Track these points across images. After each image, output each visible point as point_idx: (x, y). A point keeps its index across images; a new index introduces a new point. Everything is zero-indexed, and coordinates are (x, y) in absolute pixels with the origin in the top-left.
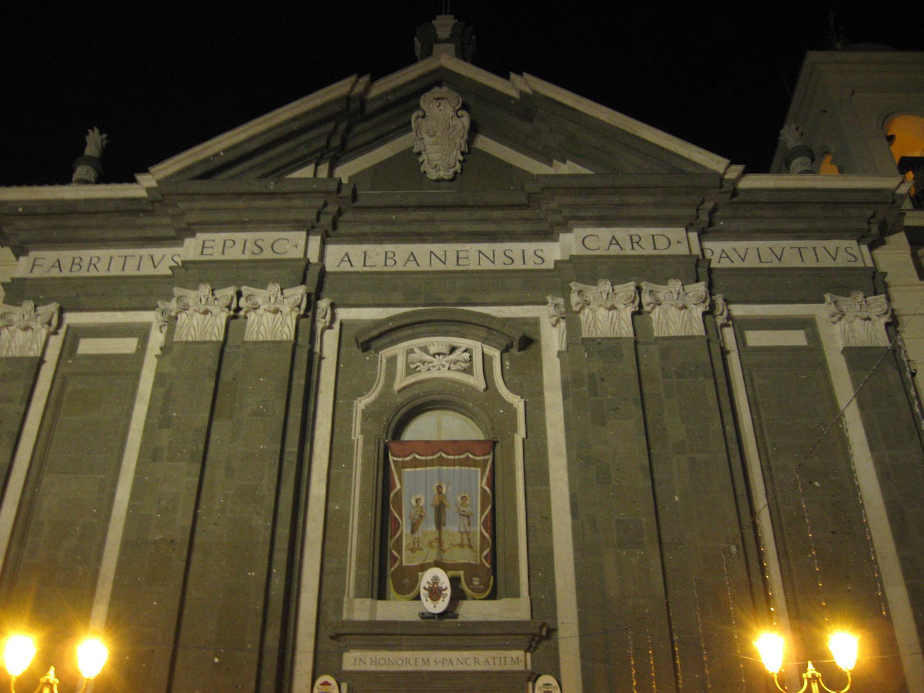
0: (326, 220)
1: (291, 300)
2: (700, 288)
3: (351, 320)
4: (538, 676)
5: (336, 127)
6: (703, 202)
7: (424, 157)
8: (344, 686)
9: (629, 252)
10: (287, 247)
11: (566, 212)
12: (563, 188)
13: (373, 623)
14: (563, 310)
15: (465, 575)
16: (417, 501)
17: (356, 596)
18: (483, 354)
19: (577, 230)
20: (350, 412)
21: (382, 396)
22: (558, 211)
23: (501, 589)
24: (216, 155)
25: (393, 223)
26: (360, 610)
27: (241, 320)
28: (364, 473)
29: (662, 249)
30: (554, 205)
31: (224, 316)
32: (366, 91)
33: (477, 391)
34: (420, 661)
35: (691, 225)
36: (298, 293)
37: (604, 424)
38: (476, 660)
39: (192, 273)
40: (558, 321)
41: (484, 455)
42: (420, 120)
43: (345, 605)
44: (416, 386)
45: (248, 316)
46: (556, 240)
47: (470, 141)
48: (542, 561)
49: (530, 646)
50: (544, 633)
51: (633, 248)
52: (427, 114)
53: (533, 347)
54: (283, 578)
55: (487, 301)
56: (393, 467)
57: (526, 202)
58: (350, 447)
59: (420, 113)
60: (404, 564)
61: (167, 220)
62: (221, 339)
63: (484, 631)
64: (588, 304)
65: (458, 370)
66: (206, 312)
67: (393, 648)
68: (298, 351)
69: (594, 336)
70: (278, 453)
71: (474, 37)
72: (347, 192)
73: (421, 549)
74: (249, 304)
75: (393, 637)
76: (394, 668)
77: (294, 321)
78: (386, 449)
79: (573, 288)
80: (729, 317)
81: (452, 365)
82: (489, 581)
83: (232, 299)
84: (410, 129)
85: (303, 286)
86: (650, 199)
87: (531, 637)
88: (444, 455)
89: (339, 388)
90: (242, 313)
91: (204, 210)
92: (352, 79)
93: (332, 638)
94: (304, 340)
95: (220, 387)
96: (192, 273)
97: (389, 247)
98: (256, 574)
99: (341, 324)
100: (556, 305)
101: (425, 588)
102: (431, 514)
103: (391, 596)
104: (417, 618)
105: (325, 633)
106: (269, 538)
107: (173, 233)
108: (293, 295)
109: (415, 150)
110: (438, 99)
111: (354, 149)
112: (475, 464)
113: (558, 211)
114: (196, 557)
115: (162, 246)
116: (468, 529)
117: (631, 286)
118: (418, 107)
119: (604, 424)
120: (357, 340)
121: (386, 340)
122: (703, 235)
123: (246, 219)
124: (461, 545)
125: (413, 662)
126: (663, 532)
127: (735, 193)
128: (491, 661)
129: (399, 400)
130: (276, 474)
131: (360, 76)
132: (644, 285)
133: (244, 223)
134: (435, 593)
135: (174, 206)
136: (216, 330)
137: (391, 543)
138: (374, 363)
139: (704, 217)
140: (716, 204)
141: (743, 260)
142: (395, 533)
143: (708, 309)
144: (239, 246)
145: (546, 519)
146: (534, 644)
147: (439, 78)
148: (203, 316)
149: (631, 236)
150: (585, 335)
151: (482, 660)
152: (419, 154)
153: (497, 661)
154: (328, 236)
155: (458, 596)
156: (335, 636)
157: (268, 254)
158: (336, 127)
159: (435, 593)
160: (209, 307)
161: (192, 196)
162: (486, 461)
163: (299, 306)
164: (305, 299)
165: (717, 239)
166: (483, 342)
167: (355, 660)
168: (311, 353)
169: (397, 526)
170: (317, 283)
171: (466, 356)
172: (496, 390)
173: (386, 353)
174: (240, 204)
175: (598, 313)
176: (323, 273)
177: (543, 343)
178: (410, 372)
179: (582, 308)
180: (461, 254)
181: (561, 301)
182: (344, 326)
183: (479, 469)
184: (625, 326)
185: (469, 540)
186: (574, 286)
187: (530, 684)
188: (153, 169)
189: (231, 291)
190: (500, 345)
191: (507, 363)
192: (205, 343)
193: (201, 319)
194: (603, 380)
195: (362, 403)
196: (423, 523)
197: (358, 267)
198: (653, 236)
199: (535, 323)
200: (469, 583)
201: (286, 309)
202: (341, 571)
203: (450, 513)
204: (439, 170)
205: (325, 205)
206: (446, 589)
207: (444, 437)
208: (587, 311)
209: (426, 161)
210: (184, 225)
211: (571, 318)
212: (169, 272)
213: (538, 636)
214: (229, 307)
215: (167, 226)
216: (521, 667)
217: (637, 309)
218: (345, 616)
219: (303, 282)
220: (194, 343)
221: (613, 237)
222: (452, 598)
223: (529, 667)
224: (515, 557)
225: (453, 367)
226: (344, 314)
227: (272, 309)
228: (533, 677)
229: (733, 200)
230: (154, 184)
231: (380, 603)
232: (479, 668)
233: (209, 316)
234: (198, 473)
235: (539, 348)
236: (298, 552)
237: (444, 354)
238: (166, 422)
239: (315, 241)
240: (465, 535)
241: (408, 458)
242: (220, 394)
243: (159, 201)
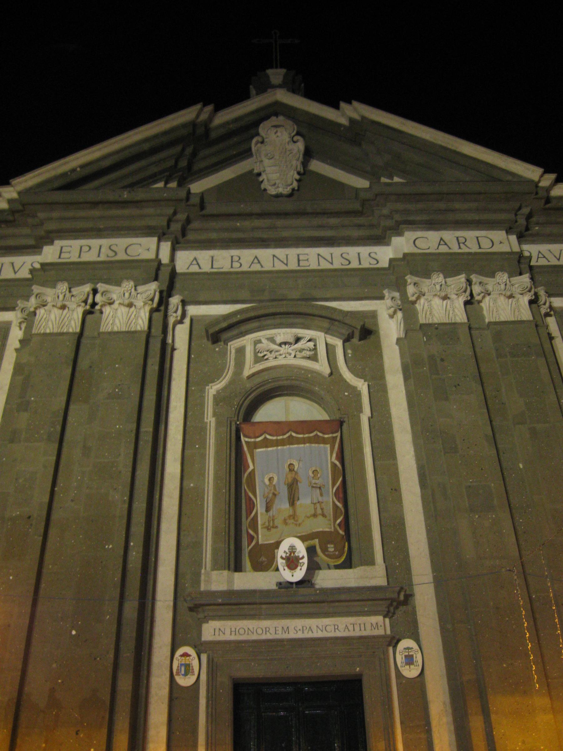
0: (176, 227)
1: (145, 296)
2: (525, 279)
3: (201, 316)
4: (398, 641)
5: (183, 150)
6: (520, 208)
7: (263, 177)
8: (204, 657)
9: (455, 249)
10: (140, 251)
11: (397, 217)
12: (395, 194)
13: (231, 593)
14: (399, 302)
15: (319, 542)
16: (270, 479)
17: (213, 569)
18: (327, 344)
19: (407, 234)
20: (202, 398)
21: (230, 383)
22: (389, 217)
23: (355, 558)
24: (73, 170)
25: (237, 230)
26: (217, 581)
27: (97, 314)
28: (217, 453)
29: (486, 246)
30: (385, 211)
31: (80, 311)
32: (211, 119)
33: (324, 377)
34: (280, 629)
35: (510, 228)
36: (152, 288)
37: (447, 399)
38: (336, 628)
39: (49, 274)
40: (395, 312)
41: (332, 433)
42: (259, 145)
43: (203, 577)
44: (264, 373)
45: (104, 310)
46: (388, 244)
47: (305, 164)
48: (394, 529)
49: (388, 612)
50: (402, 597)
51: (460, 248)
52: (266, 140)
53: (372, 337)
54: (141, 550)
55: (328, 296)
56: (245, 448)
57: (360, 209)
58: (203, 429)
59: (260, 139)
60: (260, 542)
61: (26, 231)
62: (78, 330)
63: (343, 597)
64: (424, 295)
65: (304, 358)
66: (63, 307)
67: (252, 617)
68: (152, 340)
69: (431, 322)
70: (134, 432)
71: (303, 85)
72: (195, 200)
73: (276, 527)
74: (104, 299)
75: (252, 606)
76: (254, 637)
77: (147, 314)
78: (238, 431)
79: (409, 281)
80: (551, 307)
81: (298, 353)
82: (344, 547)
83: (88, 295)
84: (251, 155)
85: (156, 282)
86: (474, 205)
87: (389, 602)
88: (294, 434)
89: (190, 376)
90: (98, 307)
91: (61, 219)
92: (198, 106)
93: (191, 609)
94: (157, 331)
95: (77, 375)
96: (49, 274)
97: (235, 252)
98: (114, 546)
99: (192, 320)
100: (392, 298)
101: (282, 557)
102: (284, 492)
103: (247, 569)
104: (274, 587)
105: (183, 606)
106: (125, 513)
107: (32, 242)
108: (146, 291)
109: (256, 171)
110: (276, 126)
111: (201, 170)
112: (324, 441)
113: (389, 217)
114: (53, 531)
115: (22, 254)
116: (320, 499)
117: (462, 278)
118: (258, 134)
119: (447, 399)
120: (207, 331)
121: (235, 332)
122: (521, 237)
123: (102, 227)
124: (315, 515)
125: (272, 630)
126: (511, 497)
127: (548, 200)
128: (351, 628)
129: (248, 385)
130: (132, 451)
131: (205, 105)
132: (474, 277)
133: (100, 230)
134: (292, 562)
135: (34, 216)
136: (73, 323)
137: (245, 523)
138: (224, 354)
139: (522, 221)
140: (531, 210)
141: (559, 260)
142: (251, 513)
143: (533, 297)
144: (95, 251)
145: (396, 490)
146: (392, 609)
147: (276, 110)
148: (61, 311)
149: (457, 238)
150: (422, 320)
151: (342, 627)
152: (259, 174)
153: (357, 628)
154: (178, 243)
155: (313, 567)
156: (194, 607)
157: (122, 256)
158: (183, 150)
159: (292, 562)
160: (66, 303)
161: (51, 205)
162: (335, 438)
163: (152, 300)
164: (157, 294)
165: (533, 242)
166: (326, 333)
167: (214, 630)
168: (164, 343)
169: (251, 505)
170: (170, 282)
171: (311, 344)
172: (341, 375)
173: (234, 345)
174: (96, 213)
175: (433, 303)
176: (173, 274)
177: (382, 333)
178: (258, 359)
179: (418, 298)
180: (301, 258)
181: (397, 295)
182: (194, 321)
183: (328, 446)
184: (459, 314)
185: (322, 509)
186: (410, 279)
187: (391, 649)
188: (14, 182)
189: (87, 288)
190: (342, 334)
191: (349, 351)
192: (62, 334)
193: (59, 313)
194: (442, 360)
195: (213, 389)
196: (277, 501)
197: (206, 268)
198: (477, 238)
199: (373, 315)
200: (324, 550)
201: (139, 303)
202: (198, 545)
203: (303, 487)
204: (278, 187)
205: (175, 213)
206: (303, 557)
207: (292, 418)
208: (422, 300)
209: (266, 181)
210: (43, 233)
211: (407, 308)
212: (30, 276)
213: (395, 601)
214: (85, 302)
215: (27, 236)
216: (381, 632)
217: (469, 298)
218: (202, 588)
219: (156, 279)
220: (51, 334)
221: (441, 239)
222: (308, 569)
223: (388, 632)
224: (368, 527)
225: (299, 355)
226: (193, 310)
227: (126, 302)
228: (394, 641)
229: (547, 206)
230: (15, 195)
231: (237, 575)
232: (338, 634)
233: (66, 311)
234: (55, 452)
235: (378, 337)
236: (155, 527)
237: (290, 344)
238: (24, 406)
239: (166, 247)
240: (318, 505)
241: (259, 439)
242: (76, 381)
243: (18, 211)
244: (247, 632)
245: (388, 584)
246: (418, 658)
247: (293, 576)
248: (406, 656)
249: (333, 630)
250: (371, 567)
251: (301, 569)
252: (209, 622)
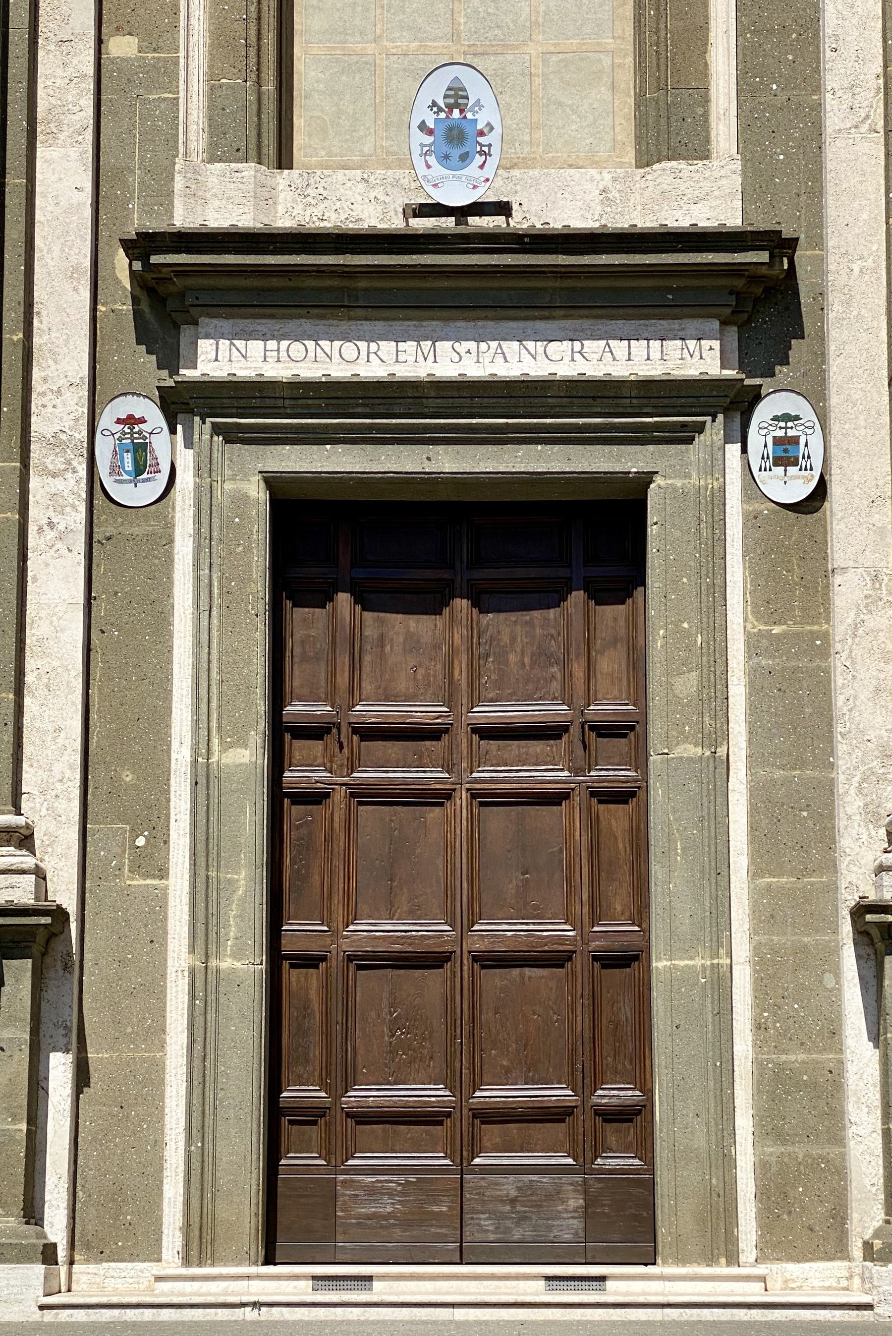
26: (220, 197)
43: (179, 183)
101: (423, 127)
244: (311, 354)
246: (812, 444)
248: (777, 441)
249: (568, 358)
250: (624, 129)
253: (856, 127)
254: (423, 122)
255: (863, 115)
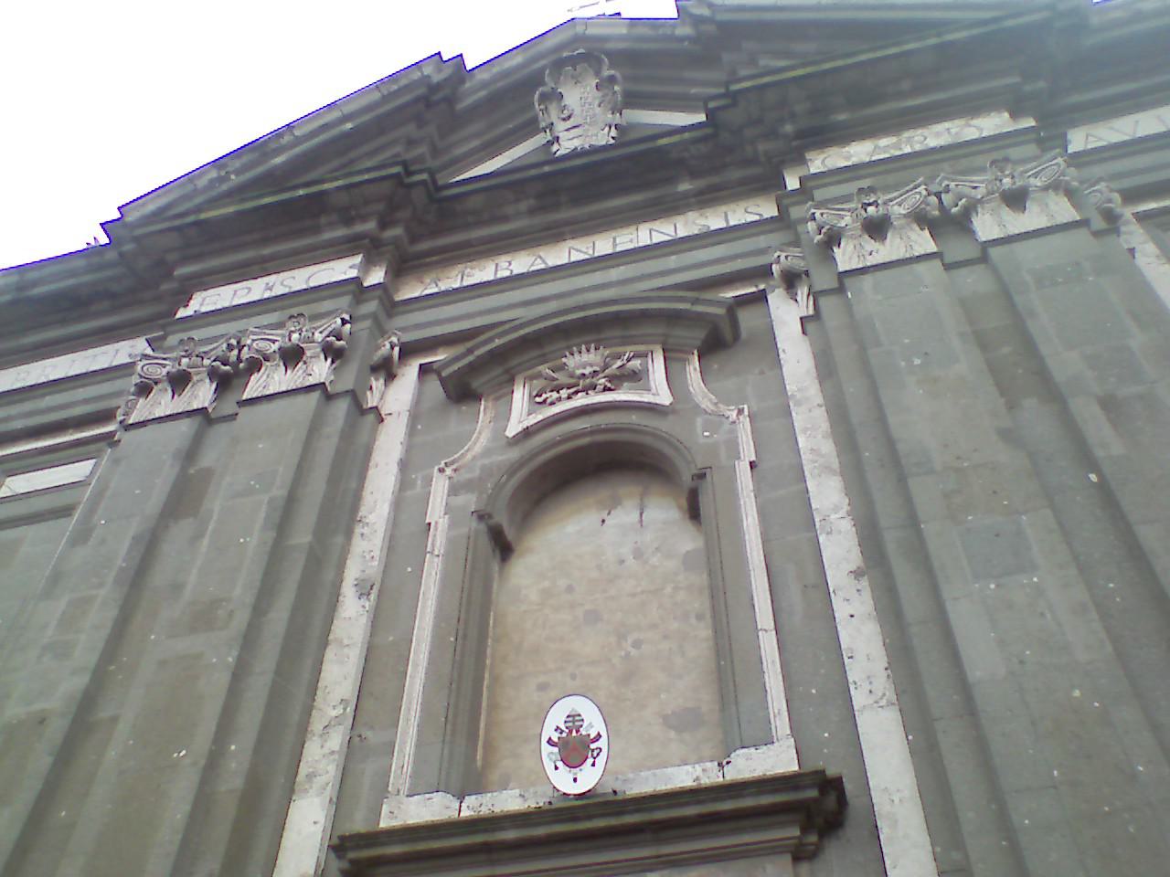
101: (550, 742)
245: (800, 768)
247: (575, 780)
251: (593, 765)
252: (809, 156)
253: (876, 702)
254: (550, 738)
255: (880, 694)
